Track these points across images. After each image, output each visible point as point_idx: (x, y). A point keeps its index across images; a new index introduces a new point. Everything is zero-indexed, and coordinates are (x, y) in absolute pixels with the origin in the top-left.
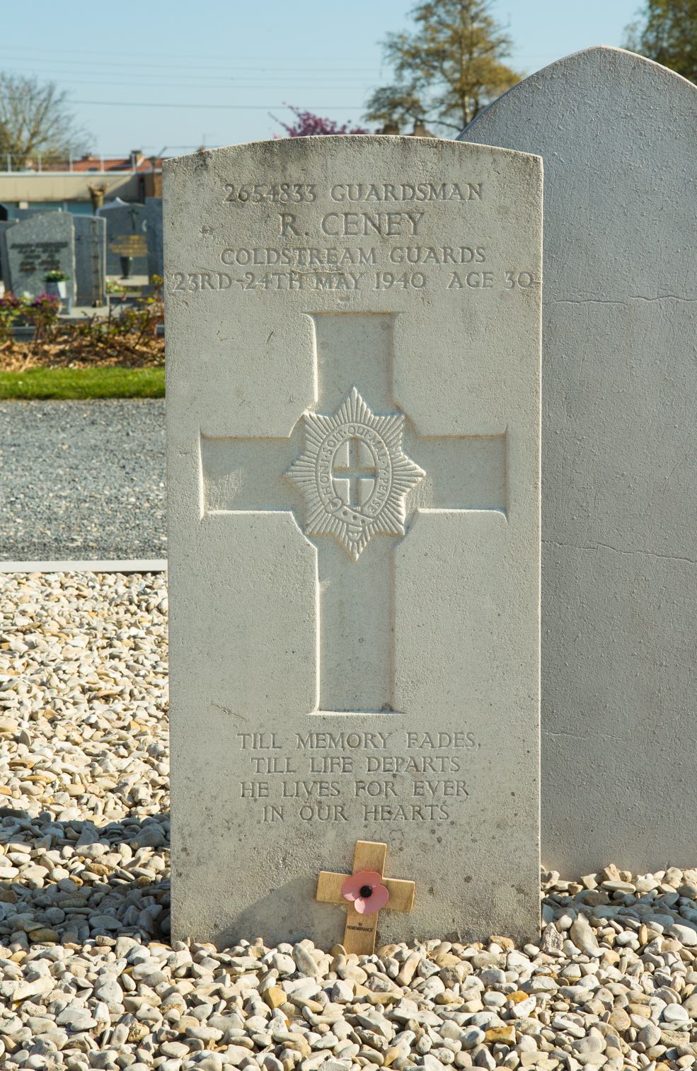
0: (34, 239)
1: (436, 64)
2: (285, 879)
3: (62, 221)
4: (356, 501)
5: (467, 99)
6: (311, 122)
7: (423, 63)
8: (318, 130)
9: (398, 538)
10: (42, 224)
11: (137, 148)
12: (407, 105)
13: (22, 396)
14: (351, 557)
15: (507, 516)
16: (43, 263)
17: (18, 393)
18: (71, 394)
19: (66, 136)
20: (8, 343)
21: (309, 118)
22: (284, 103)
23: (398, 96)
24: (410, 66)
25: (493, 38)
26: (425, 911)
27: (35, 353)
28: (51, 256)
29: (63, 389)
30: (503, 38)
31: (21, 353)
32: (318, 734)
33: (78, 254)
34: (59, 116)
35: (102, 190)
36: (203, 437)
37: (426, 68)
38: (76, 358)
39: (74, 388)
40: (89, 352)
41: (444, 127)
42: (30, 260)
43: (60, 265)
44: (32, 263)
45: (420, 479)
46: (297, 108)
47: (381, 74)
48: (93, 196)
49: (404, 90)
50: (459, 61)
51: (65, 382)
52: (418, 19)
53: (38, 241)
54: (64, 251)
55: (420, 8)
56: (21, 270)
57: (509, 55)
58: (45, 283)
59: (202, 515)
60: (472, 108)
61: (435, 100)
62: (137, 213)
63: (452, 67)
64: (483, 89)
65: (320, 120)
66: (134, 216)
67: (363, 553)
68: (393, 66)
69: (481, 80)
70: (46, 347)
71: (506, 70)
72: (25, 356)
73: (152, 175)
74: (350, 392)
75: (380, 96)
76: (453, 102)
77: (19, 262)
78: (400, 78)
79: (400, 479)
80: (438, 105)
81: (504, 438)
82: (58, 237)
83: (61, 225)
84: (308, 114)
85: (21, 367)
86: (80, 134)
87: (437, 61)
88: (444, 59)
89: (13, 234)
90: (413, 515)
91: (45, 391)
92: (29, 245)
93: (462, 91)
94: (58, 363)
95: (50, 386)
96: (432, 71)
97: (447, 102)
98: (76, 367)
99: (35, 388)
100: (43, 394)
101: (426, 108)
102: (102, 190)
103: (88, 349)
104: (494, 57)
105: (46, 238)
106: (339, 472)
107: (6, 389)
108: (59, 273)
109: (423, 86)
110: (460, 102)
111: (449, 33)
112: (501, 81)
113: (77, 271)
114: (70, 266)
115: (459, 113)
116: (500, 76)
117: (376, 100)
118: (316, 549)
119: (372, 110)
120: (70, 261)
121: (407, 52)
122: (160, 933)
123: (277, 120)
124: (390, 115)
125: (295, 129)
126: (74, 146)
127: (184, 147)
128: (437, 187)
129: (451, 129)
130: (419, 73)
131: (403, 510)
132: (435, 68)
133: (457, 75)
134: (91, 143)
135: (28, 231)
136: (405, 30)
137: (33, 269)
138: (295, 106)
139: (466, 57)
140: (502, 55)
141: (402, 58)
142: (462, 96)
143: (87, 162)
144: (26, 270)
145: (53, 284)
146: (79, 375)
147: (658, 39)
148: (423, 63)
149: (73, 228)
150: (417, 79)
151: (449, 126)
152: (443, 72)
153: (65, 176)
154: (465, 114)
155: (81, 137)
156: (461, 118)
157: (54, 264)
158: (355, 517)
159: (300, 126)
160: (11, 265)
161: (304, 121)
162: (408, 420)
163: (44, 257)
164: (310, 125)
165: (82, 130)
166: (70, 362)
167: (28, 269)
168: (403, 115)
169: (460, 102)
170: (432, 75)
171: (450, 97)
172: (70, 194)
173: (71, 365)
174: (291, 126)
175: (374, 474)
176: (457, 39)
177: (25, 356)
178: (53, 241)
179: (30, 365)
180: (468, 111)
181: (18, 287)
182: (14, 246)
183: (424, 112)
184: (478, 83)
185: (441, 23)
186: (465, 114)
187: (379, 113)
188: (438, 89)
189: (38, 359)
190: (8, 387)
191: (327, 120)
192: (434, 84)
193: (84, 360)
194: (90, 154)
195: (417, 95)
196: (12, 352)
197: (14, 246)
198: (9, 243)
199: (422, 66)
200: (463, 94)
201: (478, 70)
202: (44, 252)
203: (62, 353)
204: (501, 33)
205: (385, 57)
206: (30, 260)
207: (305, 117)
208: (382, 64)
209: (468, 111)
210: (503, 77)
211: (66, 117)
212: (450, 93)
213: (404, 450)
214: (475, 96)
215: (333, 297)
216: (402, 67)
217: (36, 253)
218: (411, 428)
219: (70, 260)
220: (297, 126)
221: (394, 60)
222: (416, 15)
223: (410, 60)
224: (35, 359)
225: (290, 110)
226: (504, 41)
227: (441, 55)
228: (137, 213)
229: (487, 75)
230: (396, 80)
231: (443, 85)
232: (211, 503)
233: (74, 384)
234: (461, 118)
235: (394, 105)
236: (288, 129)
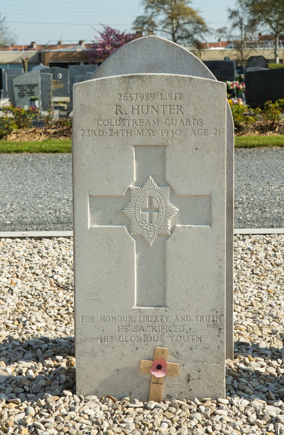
0: (24, 83)
1: (161, 6)
3: (36, 75)
4: (151, 222)
5: (174, 21)
6: (110, 30)
7: (156, 5)
8: (113, 34)
10: (28, 76)
11: (33, 41)
12: (149, 23)
13: (45, 151)
14: (149, 245)
15: (211, 227)
16: (28, 93)
17: (43, 150)
18: (64, 150)
19: (5, 36)
20: (34, 129)
21: (109, 29)
22: (98, 23)
23: (145, 20)
24: (150, 7)
27: (45, 133)
28: (31, 90)
29: (61, 148)
31: (39, 133)
33: (41, 89)
34: (2, 27)
35: (27, 59)
36: (90, 196)
37: (157, 8)
38: (62, 135)
39: (65, 148)
40: (67, 132)
41: (164, 33)
42: (23, 92)
43: (35, 94)
44: (24, 93)
45: (176, 212)
46: (104, 25)
47: (138, 10)
48: (23, 62)
49: (148, 17)
50: (171, 5)
51: (61, 145)
53: (26, 84)
54: (36, 88)
56: (19, 96)
57: (191, 2)
58: (29, 102)
59: (89, 226)
60: (176, 25)
61: (161, 21)
62: (56, 71)
63: (167, 7)
64: (181, 17)
65: (113, 29)
66: (55, 72)
67: (154, 242)
68: (144, 7)
69: (180, 13)
70: (48, 130)
71: (190, 9)
72: (41, 134)
73: (44, 53)
74: (148, 178)
75: (138, 19)
76: (168, 22)
77: (18, 92)
78: (146, 12)
80: (162, 23)
82: (34, 82)
83: (35, 77)
84: (108, 27)
85: (40, 139)
86: (11, 35)
87: (161, 5)
88: (164, 4)
89: (16, 81)
91: (54, 149)
92: (22, 86)
93: (172, 17)
94: (55, 137)
95: (55, 147)
96: (160, 9)
97: (166, 22)
98: (62, 139)
99: (50, 148)
100: (53, 150)
101: (157, 25)
102: (27, 59)
103: (66, 131)
104: (185, 4)
105: (29, 83)
106: (144, 210)
107: (38, 149)
108: (36, 97)
109: (156, 15)
110: (171, 22)
112: (188, 13)
113: (41, 96)
114: (39, 94)
115: (170, 27)
116: (188, 11)
117: (137, 21)
118: (135, 241)
119: (135, 26)
120: (39, 92)
123: (95, 30)
124: (142, 27)
125: (103, 33)
126: (8, 40)
127: (71, 41)
129: (167, 33)
130: (154, 10)
131: (169, 225)
132: (161, 8)
133: (170, 11)
134: (15, 39)
135: (22, 80)
137: (24, 95)
138: (103, 23)
139: (173, 3)
140: (188, 2)
141: (147, 4)
142: (172, 20)
143: (16, 48)
144: (21, 96)
145: (33, 102)
146: (65, 142)
148: (156, 5)
149: (40, 78)
150: (153, 13)
151: (167, 32)
152: (164, 10)
153: (8, 53)
154: (173, 27)
155: (12, 36)
156: (171, 29)
157: (32, 93)
158: (150, 228)
159: (105, 32)
160: (15, 94)
161: (107, 30)
162: (171, 189)
163: (28, 90)
164: (109, 32)
165: (12, 33)
166: (60, 136)
167: (22, 95)
168: (148, 27)
169: (171, 22)
170: (160, 11)
171: (167, 20)
172: (10, 61)
173: (60, 138)
174: (101, 32)
175: (158, 210)
177: (41, 134)
178: (32, 84)
179: (43, 138)
180: (174, 26)
181: (18, 103)
182: (16, 86)
183: (156, 26)
184: (179, 14)
186: (173, 27)
187: (138, 27)
188: (162, 17)
189: (46, 135)
190: (38, 147)
191: (116, 29)
192: (160, 14)
193: (65, 136)
194: (14, 43)
195: (153, 19)
196: (36, 133)
197: (16, 86)
198: (14, 85)
199: (156, 7)
200: (172, 18)
201: (179, 8)
202: (28, 88)
203: (55, 133)
205: (140, 3)
206: (23, 92)
207: (107, 28)
208: (139, 6)
209: (174, 26)
210: (189, 11)
211: (5, 28)
212: (167, 18)
213: (170, 201)
214: (177, 20)
216: (147, 7)
217: (25, 89)
219: (38, 92)
220: (104, 32)
221: (144, 4)
223: (151, 5)
224: (45, 135)
225: (101, 26)
228: (56, 71)
229: (183, 11)
230: (145, 13)
231: (164, 15)
233: (65, 146)
234: (171, 29)
235: (144, 23)
236: (100, 34)
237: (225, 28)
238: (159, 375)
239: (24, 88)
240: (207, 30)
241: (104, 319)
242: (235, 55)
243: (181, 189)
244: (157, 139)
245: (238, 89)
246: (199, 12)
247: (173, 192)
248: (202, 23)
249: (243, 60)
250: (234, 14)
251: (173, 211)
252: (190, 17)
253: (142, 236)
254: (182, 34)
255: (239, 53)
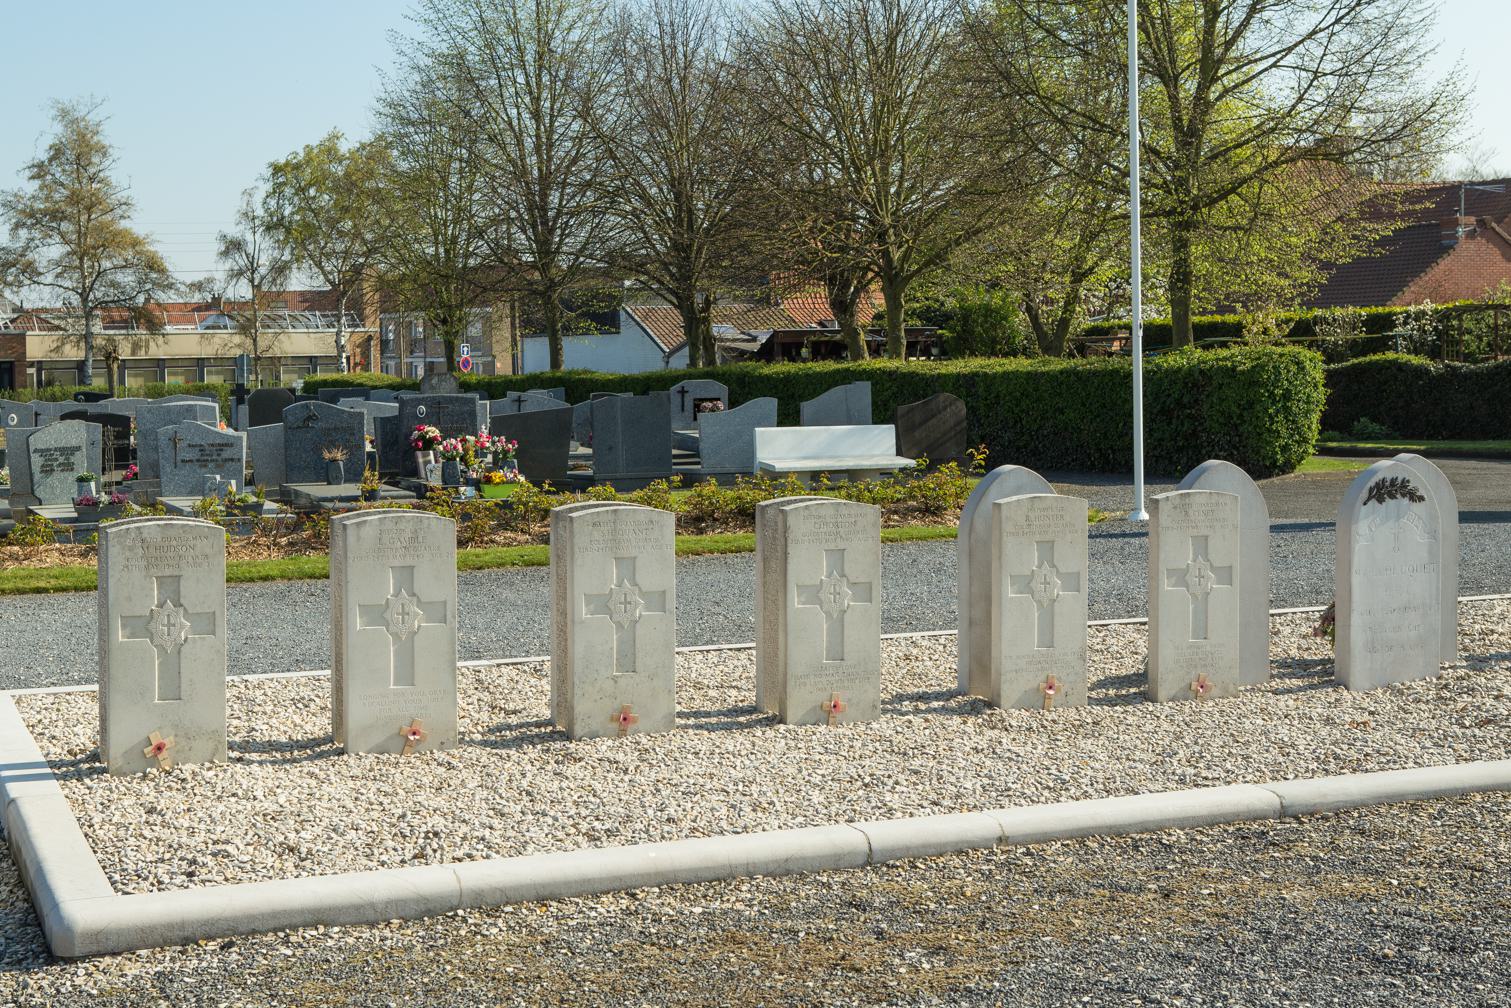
0: (53, 444)
2: (1183, 685)
9: (416, 633)
16: (59, 465)
25: (113, 200)
26: (1215, 692)
30: (122, 201)
32: (1191, 646)
52: (33, 178)
55: (33, 166)
56: (42, 472)
68: (8, 227)
71: (125, 233)
72: (269, 548)
79: (182, 627)
81: (664, 592)
82: (74, 443)
90: (419, 627)
92: (49, 450)
106: (163, 625)
111: (66, 192)
121: (23, 211)
122: (1154, 701)
128: (1217, 504)
136: (20, 189)
140: (122, 217)
147: (280, 207)
163: (61, 459)
175: (174, 625)
176: (74, 199)
182: (36, 451)
185: (55, 182)
188: (52, 251)
197: (36, 451)
198: (32, 449)
201: (101, 228)
204: (122, 196)
215: (1195, 532)
216: (18, 226)
218: (1211, 565)
222: (28, 173)
226: (125, 204)
227: (56, 215)
232: (123, 637)
237: (210, 280)
238: (1051, 692)
239: (52, 455)
240: (170, 286)
241: (1018, 657)
242: (239, 346)
243: (1062, 570)
244: (1048, 538)
245: (506, 452)
246: (151, 243)
247: (1058, 571)
248: (162, 271)
249: (258, 358)
250: (233, 246)
251: (418, 614)
252: (129, 254)
253: (397, 634)
254: (106, 294)
255: (249, 342)
